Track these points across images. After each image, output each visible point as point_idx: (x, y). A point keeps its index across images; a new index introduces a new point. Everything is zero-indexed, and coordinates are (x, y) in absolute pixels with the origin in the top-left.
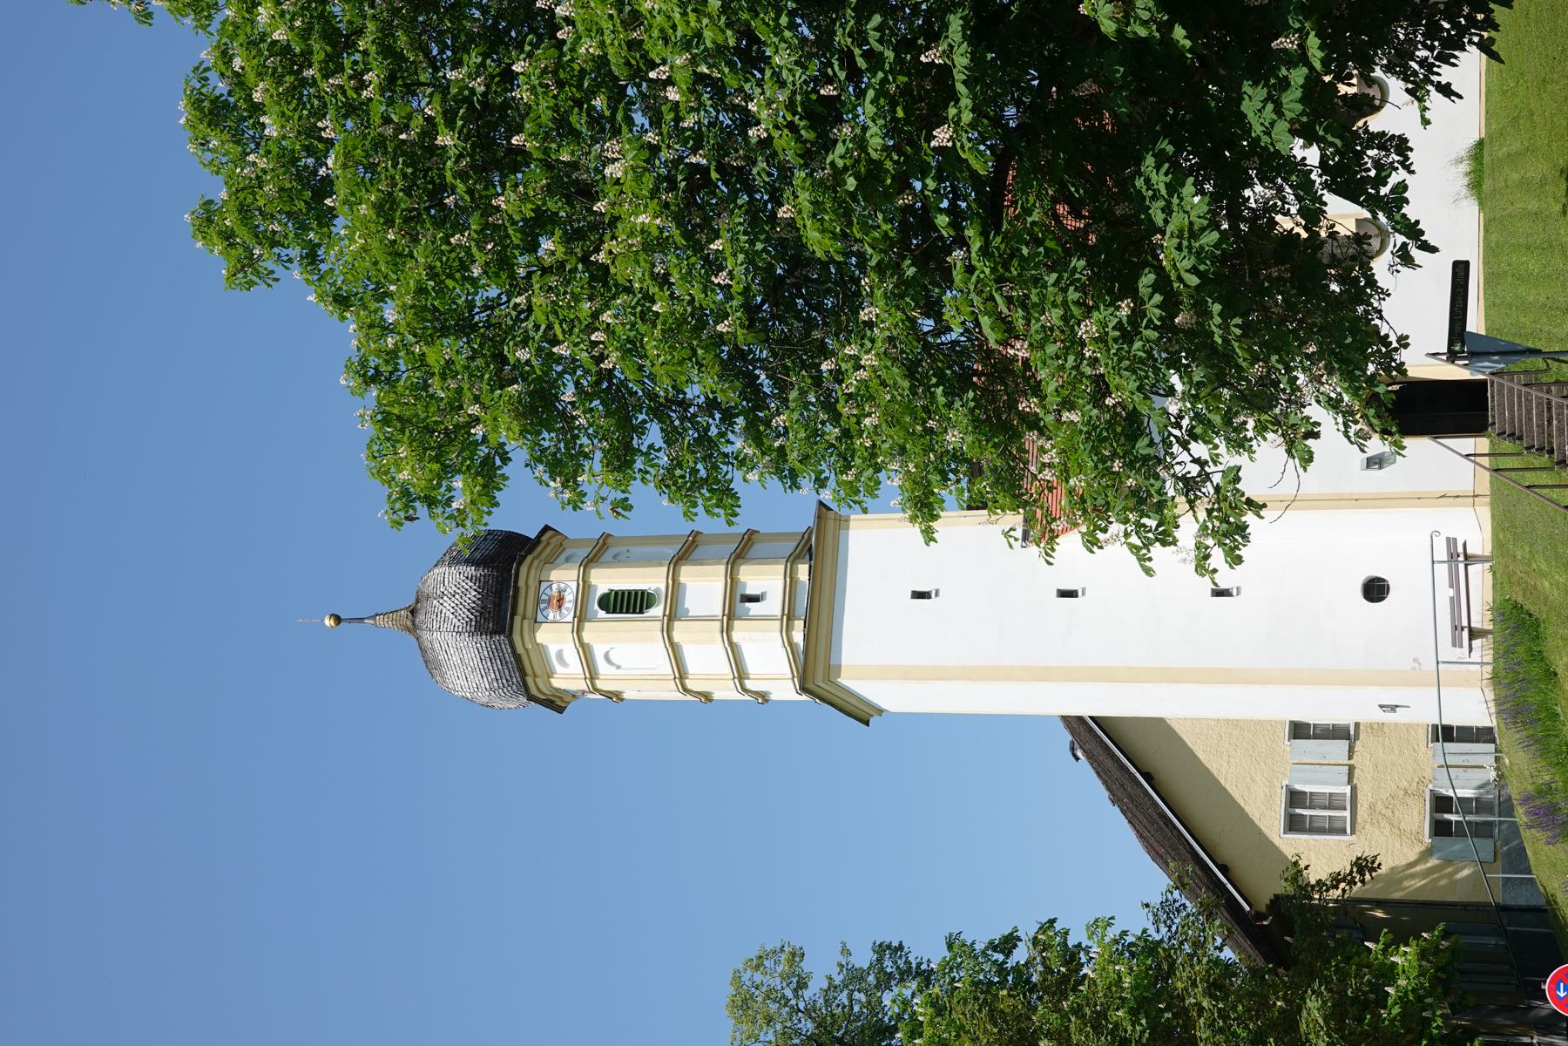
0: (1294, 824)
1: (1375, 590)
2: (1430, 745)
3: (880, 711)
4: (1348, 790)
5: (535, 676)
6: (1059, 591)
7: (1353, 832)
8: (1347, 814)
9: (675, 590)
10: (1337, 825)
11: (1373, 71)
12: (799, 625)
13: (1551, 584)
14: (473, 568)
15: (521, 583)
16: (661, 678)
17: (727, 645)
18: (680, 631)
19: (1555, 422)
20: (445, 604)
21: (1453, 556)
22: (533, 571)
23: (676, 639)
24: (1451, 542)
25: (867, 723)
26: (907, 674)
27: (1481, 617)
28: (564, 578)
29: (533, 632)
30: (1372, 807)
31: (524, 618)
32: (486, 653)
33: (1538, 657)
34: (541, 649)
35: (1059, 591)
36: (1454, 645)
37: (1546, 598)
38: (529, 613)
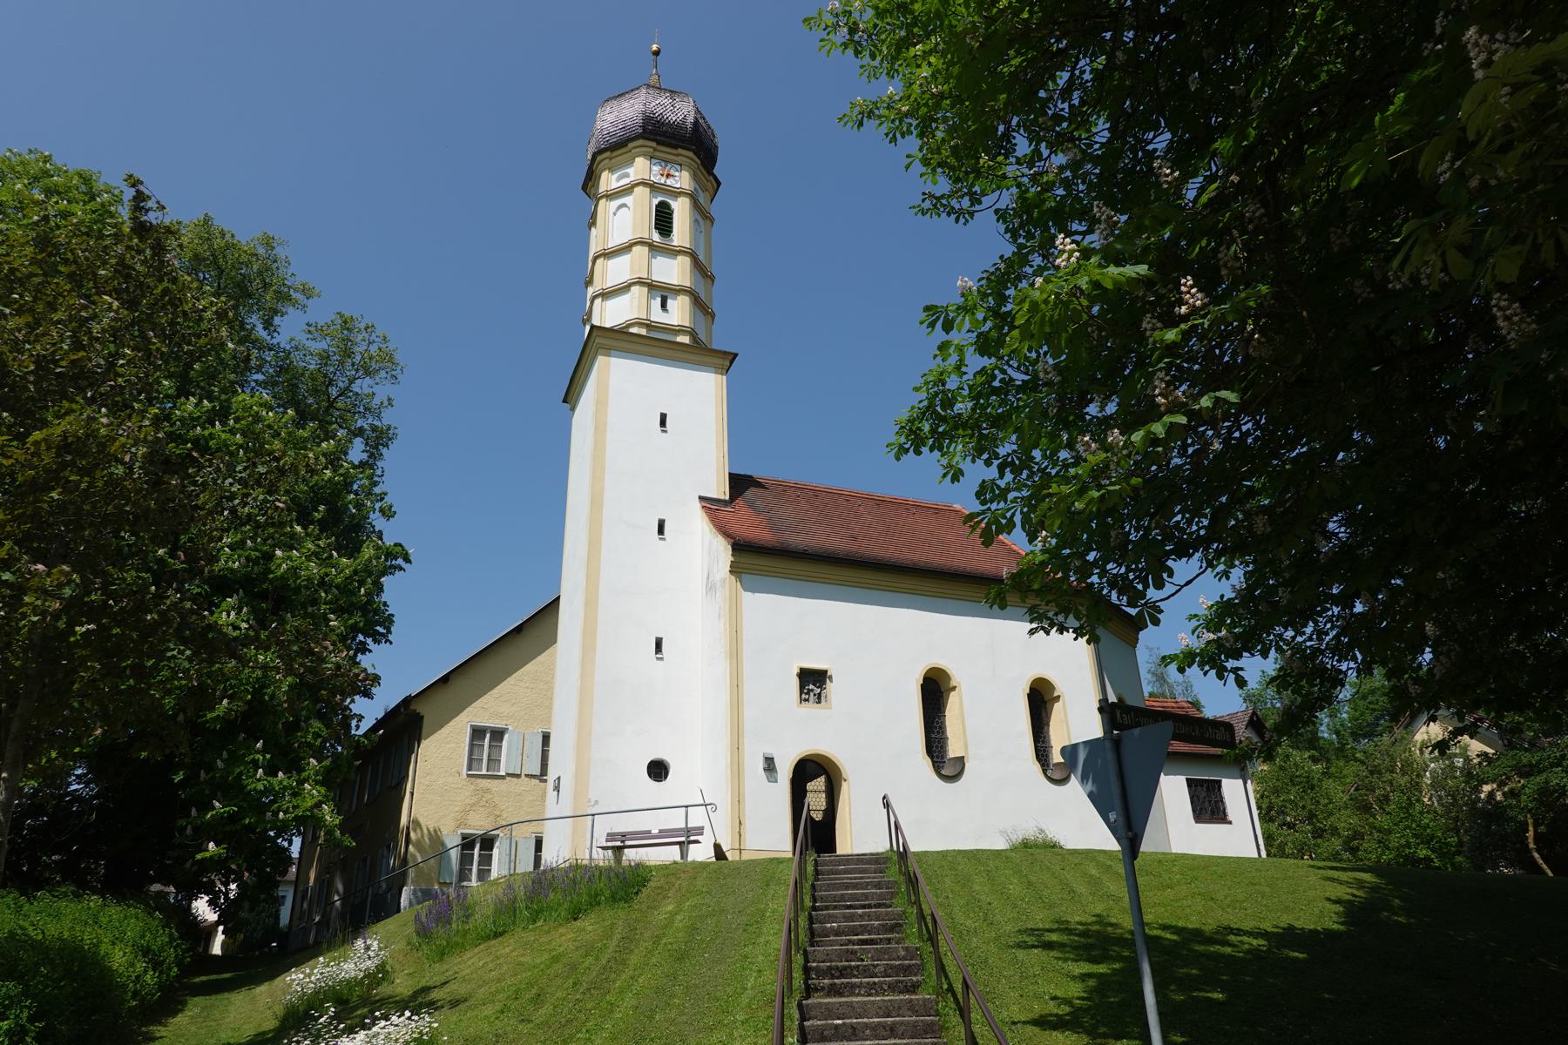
0: (478, 733)
1: (658, 770)
2: (534, 835)
3: (573, 409)
4: (502, 773)
5: (611, 159)
6: (664, 521)
7: (469, 776)
8: (484, 772)
9: (673, 252)
10: (475, 764)
12: (643, 332)
13: (670, 912)
15: (680, 151)
16: (605, 239)
18: (640, 252)
19: (860, 911)
21: (688, 831)
23: (635, 249)
25: (565, 401)
26: (600, 428)
27: (631, 855)
28: (682, 180)
29: (644, 155)
30: (488, 790)
31: (655, 150)
33: (594, 902)
34: (631, 162)
35: (664, 521)
36: (608, 835)
37: (655, 908)
38: (657, 154)
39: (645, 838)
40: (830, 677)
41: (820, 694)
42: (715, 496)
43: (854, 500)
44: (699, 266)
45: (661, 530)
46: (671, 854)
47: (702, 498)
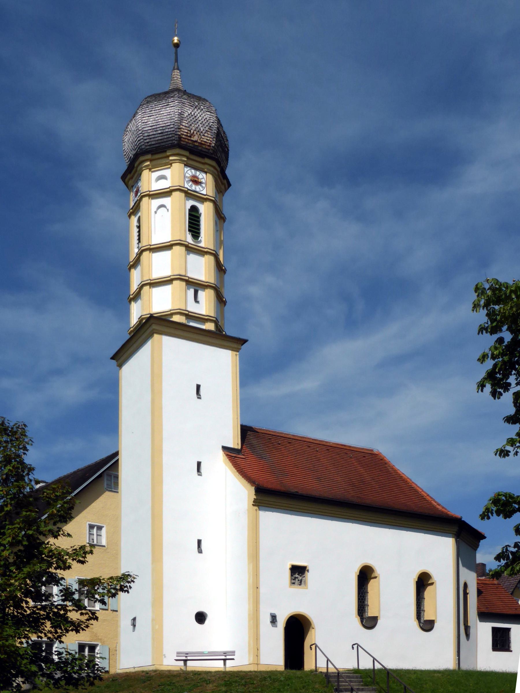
1: (201, 618)
2: (77, 642)
9: (201, 252)
11: (22, 603)
14: (216, 132)
22: (212, 169)
25: (113, 358)
29: (181, 161)
32: (167, 130)
39: (201, 656)
40: (308, 571)
41: (301, 580)
42: (231, 445)
44: (220, 268)
47: (225, 448)
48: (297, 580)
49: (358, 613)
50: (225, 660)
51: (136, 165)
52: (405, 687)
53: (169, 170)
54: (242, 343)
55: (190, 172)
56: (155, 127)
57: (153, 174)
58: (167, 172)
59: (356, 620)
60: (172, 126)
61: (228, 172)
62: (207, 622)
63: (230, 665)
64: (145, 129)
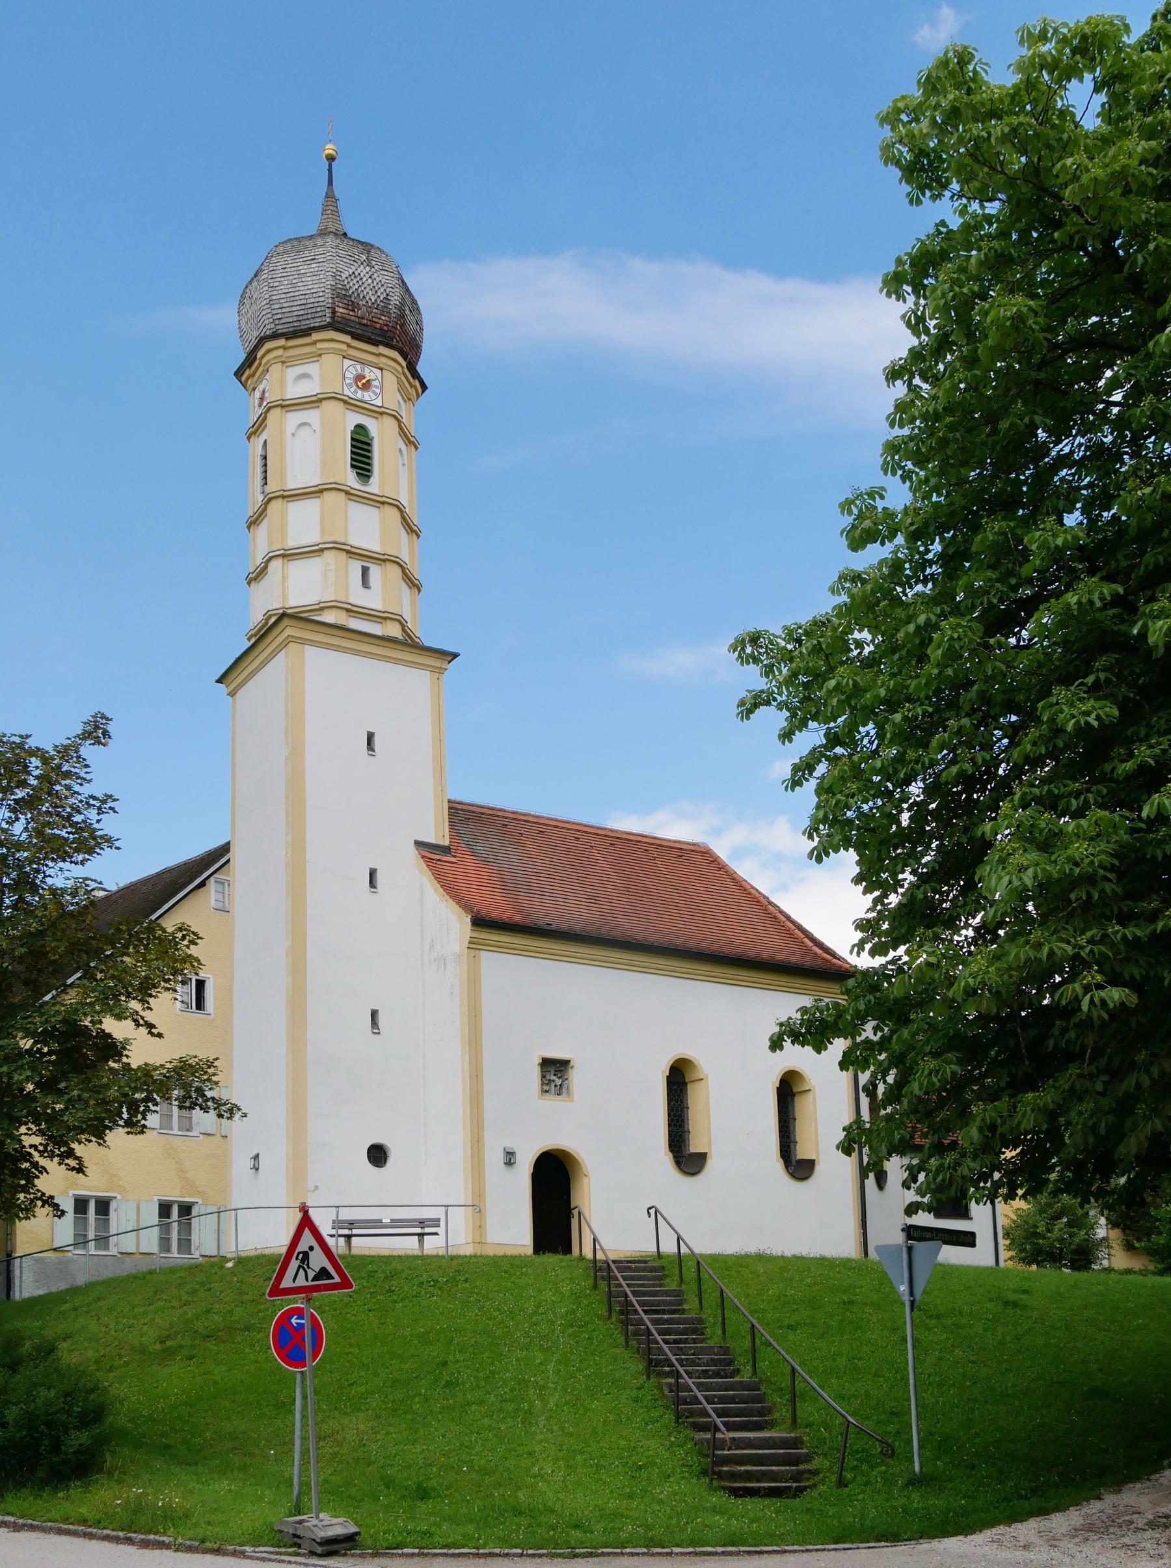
1: (378, 1155)
2: (156, 1198)
15: (382, 349)
17: (321, 546)
20: (362, 267)
21: (422, 1223)
24: (435, 1222)
25: (219, 681)
32: (312, 300)
42: (431, 840)
43: (584, 837)
45: (372, 882)
46: (409, 1245)
47: (418, 844)
48: (553, 1085)
49: (670, 1146)
50: (421, 1236)
51: (259, 356)
52: (722, 1291)
53: (317, 365)
54: (450, 659)
55: (352, 370)
56: (292, 294)
57: (289, 370)
58: (312, 369)
59: (666, 1159)
60: (321, 294)
61: (420, 368)
62: (391, 1162)
63: (433, 1245)
64: (274, 298)
